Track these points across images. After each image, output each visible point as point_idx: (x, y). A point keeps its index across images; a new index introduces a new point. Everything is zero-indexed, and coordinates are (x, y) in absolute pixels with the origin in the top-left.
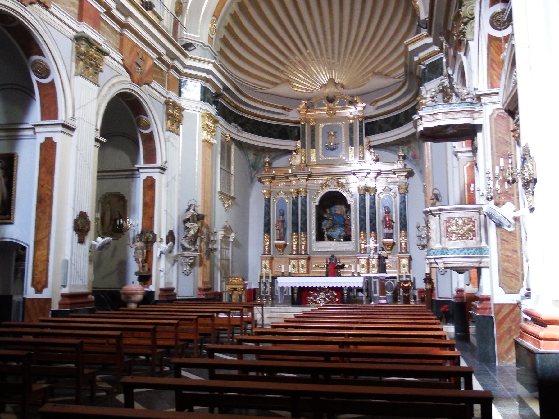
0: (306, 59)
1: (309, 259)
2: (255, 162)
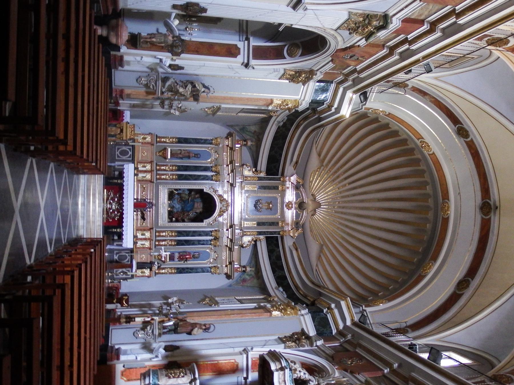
0: (340, 182)
1: (151, 181)
2: (247, 131)
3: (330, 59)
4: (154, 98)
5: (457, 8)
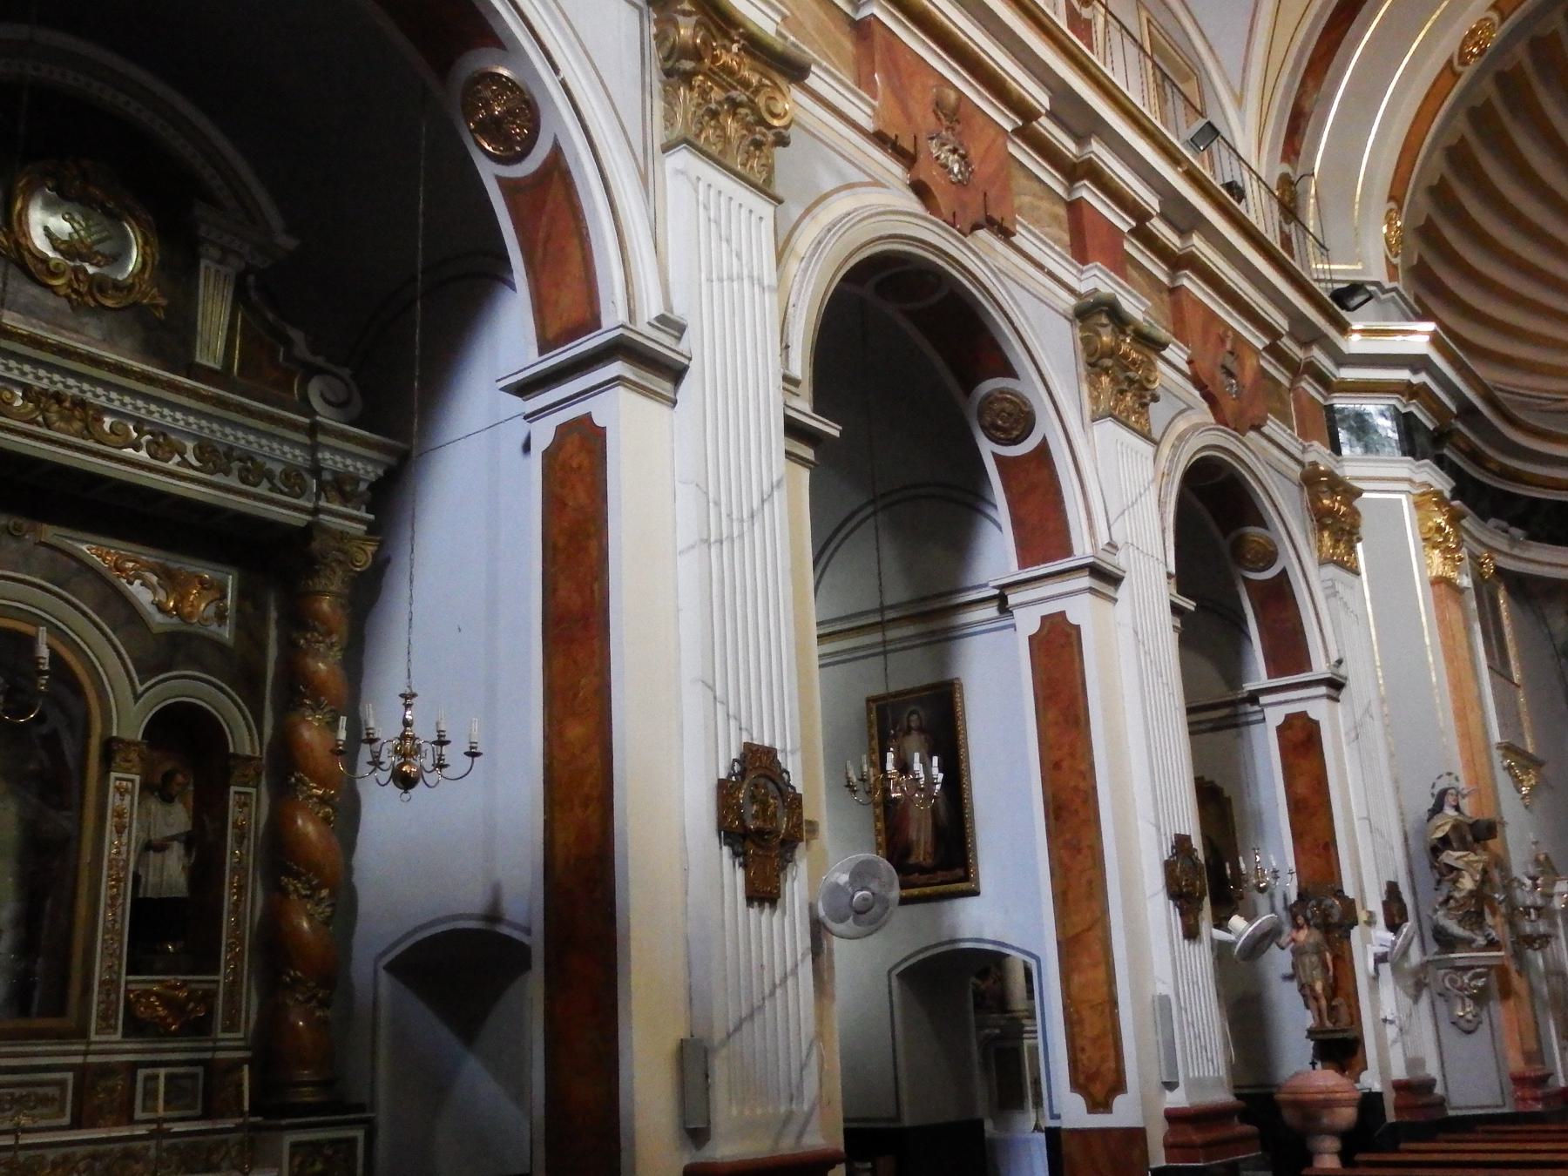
3: (1252, 434)
4: (1519, 973)
5: (1009, 128)
